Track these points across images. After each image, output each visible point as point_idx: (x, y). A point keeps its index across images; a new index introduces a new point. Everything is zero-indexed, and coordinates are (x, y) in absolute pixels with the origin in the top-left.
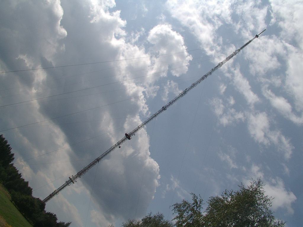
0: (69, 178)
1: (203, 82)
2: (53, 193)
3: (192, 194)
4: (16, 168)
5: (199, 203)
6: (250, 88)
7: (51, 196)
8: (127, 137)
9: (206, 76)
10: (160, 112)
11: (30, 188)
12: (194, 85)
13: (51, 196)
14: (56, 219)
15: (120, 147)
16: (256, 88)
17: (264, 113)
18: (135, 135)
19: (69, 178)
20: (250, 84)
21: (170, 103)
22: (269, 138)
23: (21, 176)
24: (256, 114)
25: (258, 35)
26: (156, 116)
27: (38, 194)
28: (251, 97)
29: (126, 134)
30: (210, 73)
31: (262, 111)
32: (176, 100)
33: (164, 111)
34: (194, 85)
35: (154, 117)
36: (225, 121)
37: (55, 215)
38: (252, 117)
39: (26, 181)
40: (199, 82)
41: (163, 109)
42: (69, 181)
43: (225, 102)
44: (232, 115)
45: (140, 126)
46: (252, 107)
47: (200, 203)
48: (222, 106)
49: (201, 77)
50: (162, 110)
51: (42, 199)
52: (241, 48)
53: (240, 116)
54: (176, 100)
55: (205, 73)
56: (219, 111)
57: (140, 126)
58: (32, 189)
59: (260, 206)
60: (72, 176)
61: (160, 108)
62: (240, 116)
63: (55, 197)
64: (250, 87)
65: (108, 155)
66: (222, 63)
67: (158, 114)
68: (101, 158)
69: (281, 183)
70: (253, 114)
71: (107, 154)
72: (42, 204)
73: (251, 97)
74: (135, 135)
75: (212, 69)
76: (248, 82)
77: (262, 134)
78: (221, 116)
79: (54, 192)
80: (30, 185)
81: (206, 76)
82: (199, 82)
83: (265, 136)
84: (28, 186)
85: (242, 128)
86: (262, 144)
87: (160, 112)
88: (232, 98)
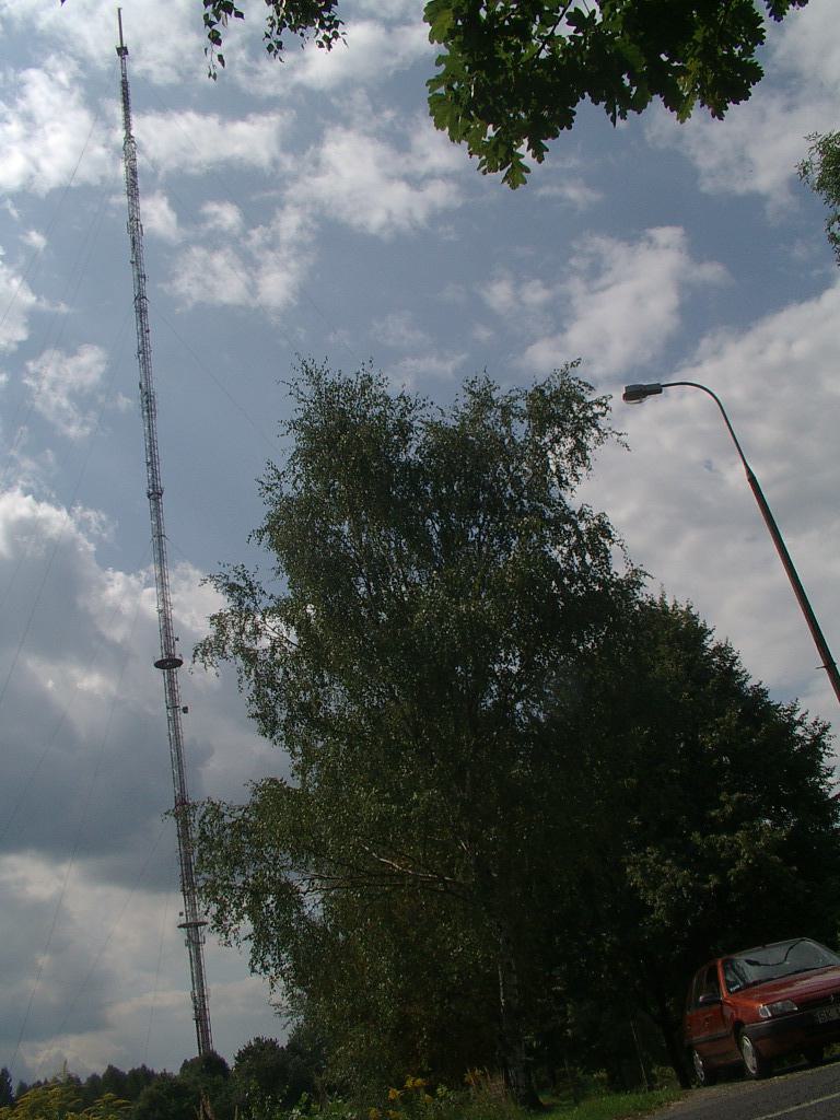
0: (180, 927)
1: (151, 320)
2: (196, 1008)
3: (205, 581)
4: (43, 1081)
5: (242, 583)
6: (221, 123)
7: (201, 1018)
8: (169, 668)
9: (140, 297)
10: (157, 512)
11: (133, 1073)
12: (143, 352)
13: (201, 1018)
14: (272, 1044)
15: (185, 710)
16: (233, 104)
17: (329, 133)
18: (177, 639)
19: (180, 927)
20: (203, 110)
21: (148, 464)
22: (431, 176)
23: (78, 1080)
24: (316, 163)
25: (119, 46)
26: (160, 536)
27: (171, 1055)
28: (252, 139)
29: (159, 665)
30: (141, 276)
31: (318, 138)
32: (151, 440)
33: (164, 499)
34: (143, 352)
35: (160, 543)
36: (276, 285)
37: (258, 1039)
38: (323, 185)
39: (101, 1071)
40: (144, 332)
41: (155, 500)
42: (189, 936)
43: (214, 241)
44: (272, 246)
45: (161, 607)
46: (288, 163)
47: (244, 578)
48: (219, 261)
49: (134, 316)
50: (157, 504)
51: (193, 1052)
52: (126, 128)
53: (290, 223)
54: (151, 440)
55: (131, 294)
56: (230, 287)
57: (161, 607)
58: (144, 1067)
59: (593, 430)
60: (181, 914)
61: (146, 504)
62: (290, 223)
63: (213, 1014)
64: (213, 121)
65: (186, 759)
66: (131, 220)
67: (159, 525)
68: (182, 790)
69: (601, 243)
70: (309, 174)
71: (180, 763)
72: (209, 1063)
73: (252, 139)
74: (177, 639)
75: (132, 263)
76: (191, 115)
77: (401, 191)
78: (253, 289)
79: (195, 1002)
80: (126, 1069)
81: (140, 297)
82: (144, 332)
83: (415, 182)
84: (123, 1074)
85: (333, 238)
86: (438, 217)
87: (157, 512)
88: (212, 208)
